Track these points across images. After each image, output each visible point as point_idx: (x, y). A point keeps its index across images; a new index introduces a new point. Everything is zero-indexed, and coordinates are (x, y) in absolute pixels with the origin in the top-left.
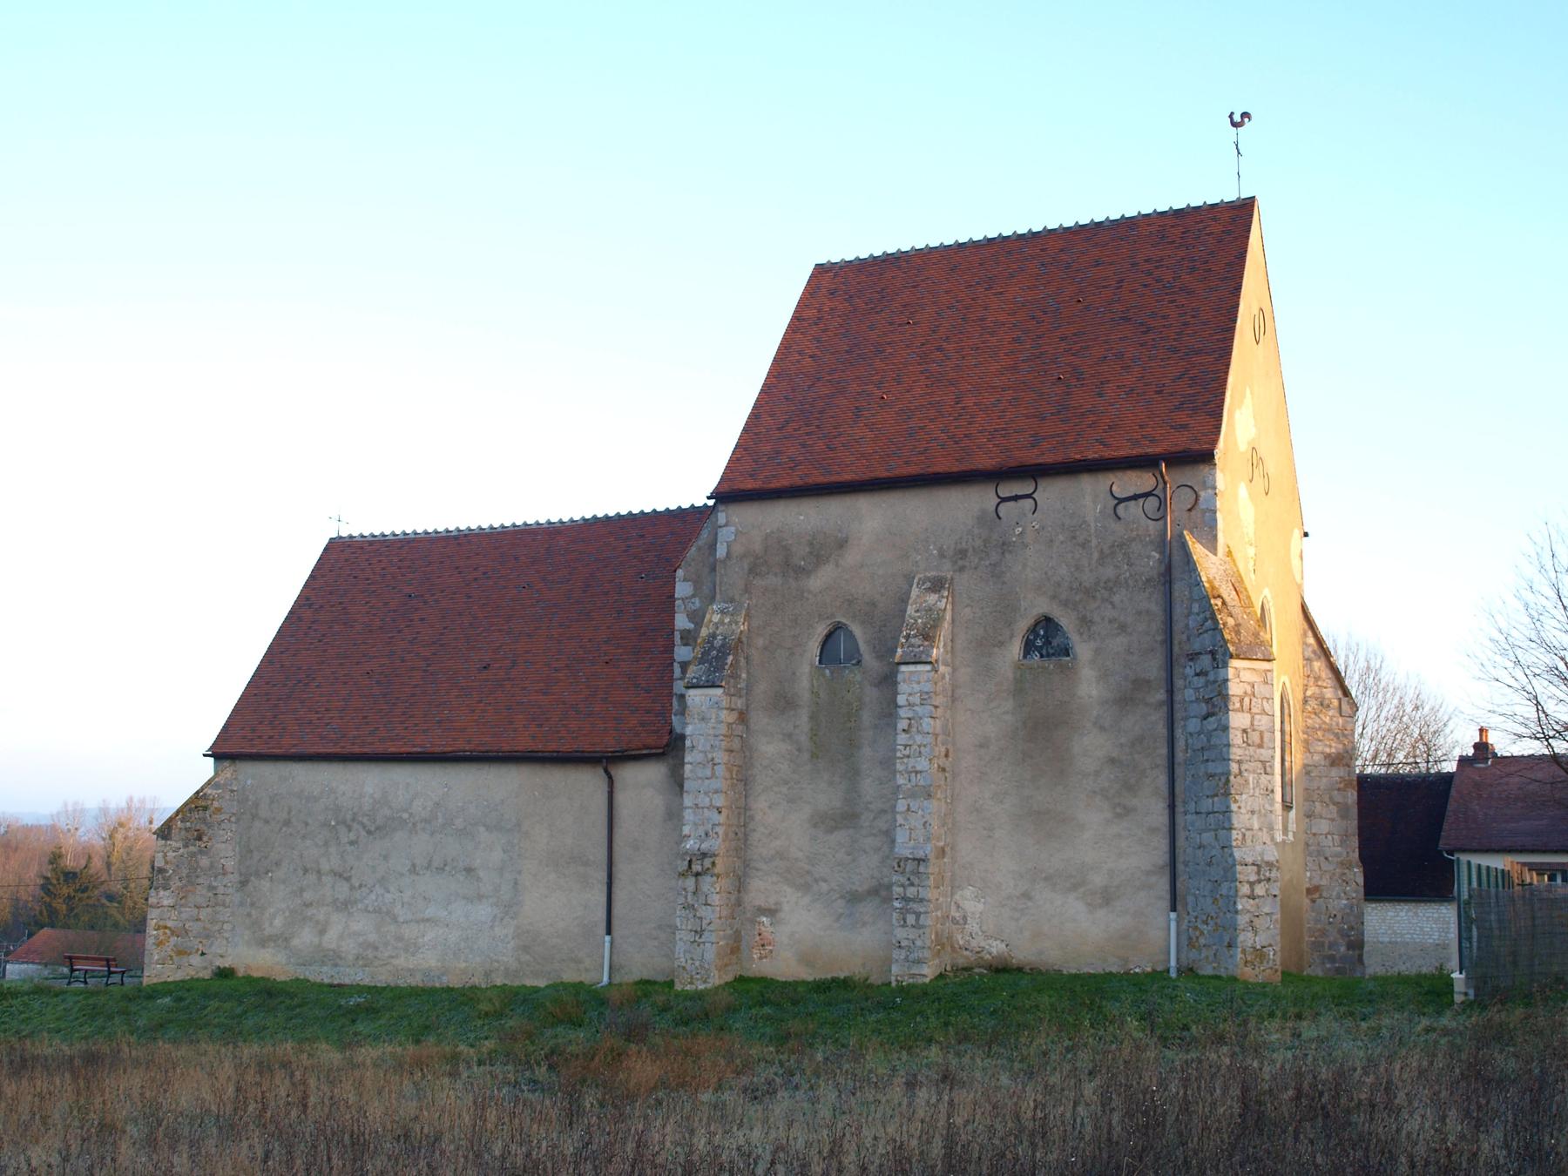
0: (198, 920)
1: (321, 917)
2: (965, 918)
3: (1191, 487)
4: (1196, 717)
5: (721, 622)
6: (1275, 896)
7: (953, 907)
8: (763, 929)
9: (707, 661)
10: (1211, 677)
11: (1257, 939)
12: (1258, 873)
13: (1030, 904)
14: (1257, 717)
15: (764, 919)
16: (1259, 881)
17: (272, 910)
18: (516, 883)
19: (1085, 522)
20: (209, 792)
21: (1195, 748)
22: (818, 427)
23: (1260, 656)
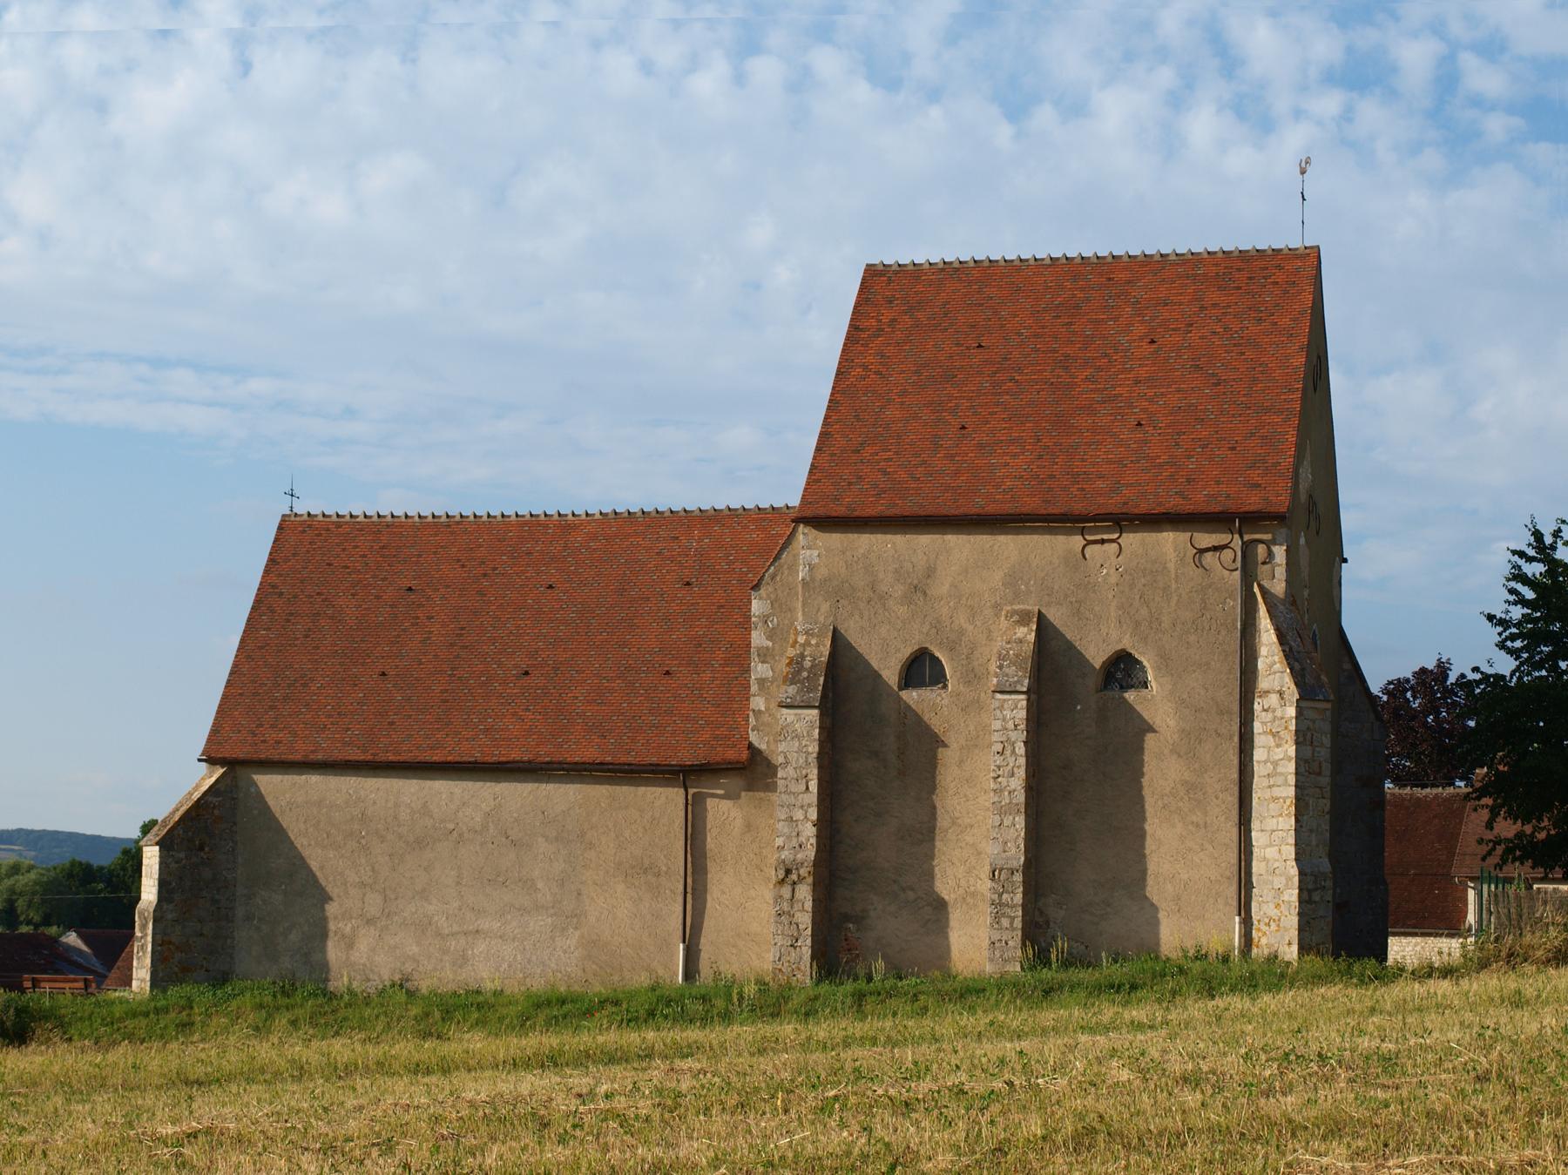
0: (201, 935)
1: (348, 929)
2: (1047, 923)
3: (1193, 546)
4: (1264, 747)
5: (807, 643)
6: (1328, 902)
7: (1037, 913)
8: (849, 935)
9: (799, 681)
10: (1278, 713)
11: (1313, 937)
12: (1315, 882)
13: (1109, 909)
14: (1317, 749)
15: (851, 925)
16: (1316, 889)
17: (287, 925)
18: (579, 894)
19: (1165, 568)
20: (210, 799)
21: (1261, 774)
22: (896, 453)
23: (1321, 697)
